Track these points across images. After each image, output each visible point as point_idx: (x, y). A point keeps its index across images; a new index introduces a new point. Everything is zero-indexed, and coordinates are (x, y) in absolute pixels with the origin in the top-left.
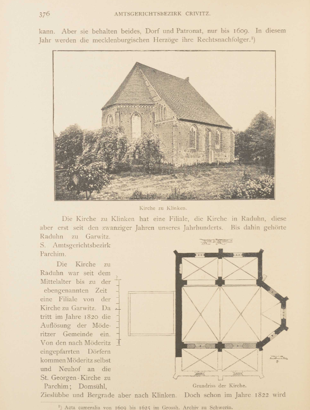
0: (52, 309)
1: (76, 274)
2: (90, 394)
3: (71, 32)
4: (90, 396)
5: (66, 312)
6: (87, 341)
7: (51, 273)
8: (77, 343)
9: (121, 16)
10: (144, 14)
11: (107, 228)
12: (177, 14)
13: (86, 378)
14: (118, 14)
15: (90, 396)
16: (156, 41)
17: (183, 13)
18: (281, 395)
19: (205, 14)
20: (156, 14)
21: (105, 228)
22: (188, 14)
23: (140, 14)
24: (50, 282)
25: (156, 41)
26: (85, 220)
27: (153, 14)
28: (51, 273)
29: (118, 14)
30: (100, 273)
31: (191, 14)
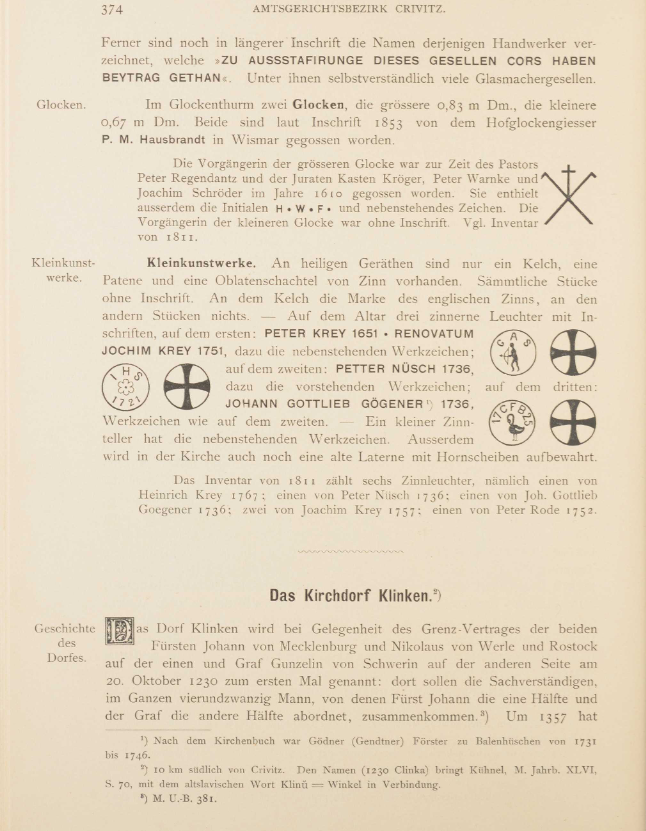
0: (204, 458)
1: (381, 318)
2: (199, 119)
3: (170, 682)
4: (199, 124)
6: (354, 295)
7: (162, 496)
8: (293, 282)
9: (265, 13)
12: (379, 9)
13: (190, 458)
14: (260, 9)
15: (199, 124)
17: (390, 8)
19: (435, 9)
20: (337, 9)
22: (400, 9)
23: (305, 9)
27: (331, 9)
28: (162, 496)
29: (260, 9)
31: (406, 9)
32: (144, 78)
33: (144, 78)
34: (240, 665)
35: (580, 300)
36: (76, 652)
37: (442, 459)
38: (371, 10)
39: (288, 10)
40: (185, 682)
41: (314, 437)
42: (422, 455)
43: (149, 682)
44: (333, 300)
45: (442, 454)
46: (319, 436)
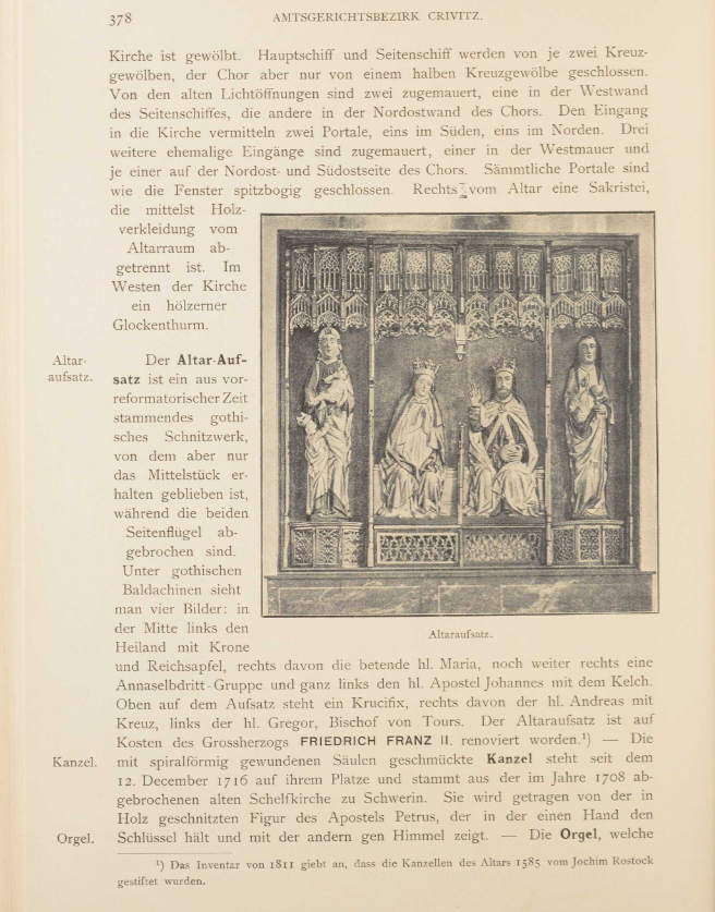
2: (128, 587)
4: (128, 592)
5: (363, 788)
6: (154, 471)
9: (286, 22)
10: (339, 17)
11: (298, 133)
12: (410, 17)
13: (214, 288)
16: (121, 649)
17: (423, 16)
18: (493, 798)
20: (365, 17)
21: (292, 133)
22: (433, 16)
23: (329, 17)
24: (166, 211)
25: (121, 649)
26: (177, 134)
27: (358, 17)
29: (281, 16)
30: (305, 172)
31: (440, 16)
32: (405, 741)
33: (405, 741)
34: (273, 725)
35: (201, 172)
36: (126, 522)
37: (217, 211)
38: (402, 18)
39: (311, 19)
40: (212, 783)
41: (585, 88)
42: (644, 698)
43: (460, 761)
44: (144, 134)
45: (217, 206)
46: (591, 87)
